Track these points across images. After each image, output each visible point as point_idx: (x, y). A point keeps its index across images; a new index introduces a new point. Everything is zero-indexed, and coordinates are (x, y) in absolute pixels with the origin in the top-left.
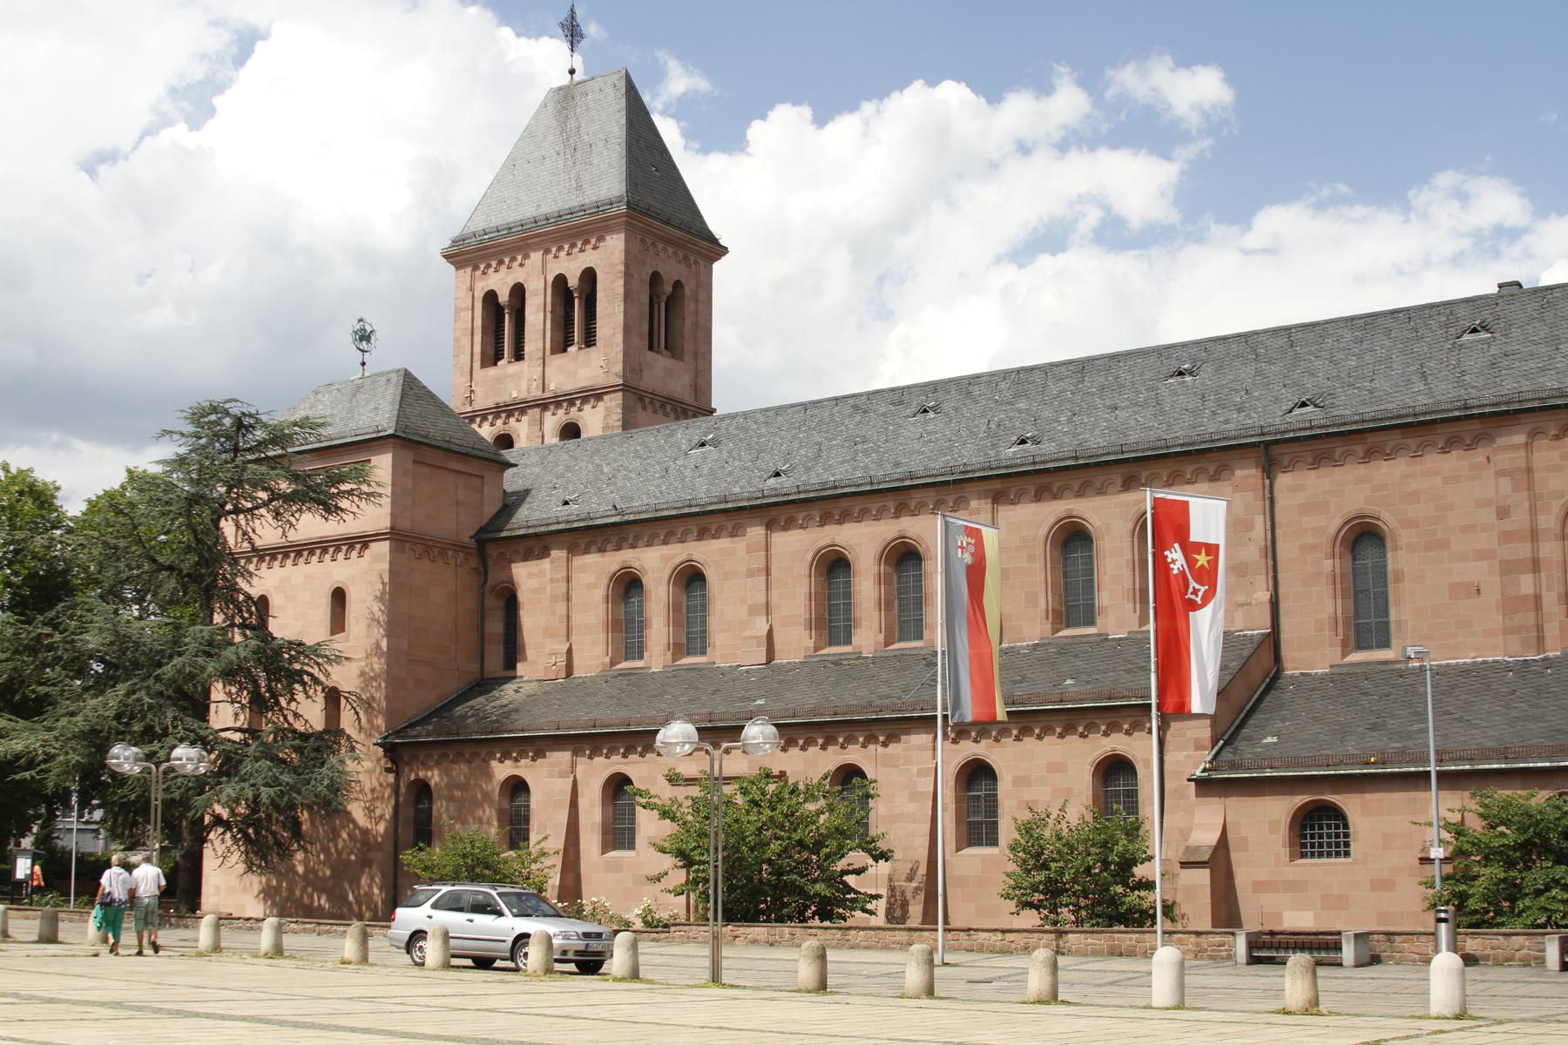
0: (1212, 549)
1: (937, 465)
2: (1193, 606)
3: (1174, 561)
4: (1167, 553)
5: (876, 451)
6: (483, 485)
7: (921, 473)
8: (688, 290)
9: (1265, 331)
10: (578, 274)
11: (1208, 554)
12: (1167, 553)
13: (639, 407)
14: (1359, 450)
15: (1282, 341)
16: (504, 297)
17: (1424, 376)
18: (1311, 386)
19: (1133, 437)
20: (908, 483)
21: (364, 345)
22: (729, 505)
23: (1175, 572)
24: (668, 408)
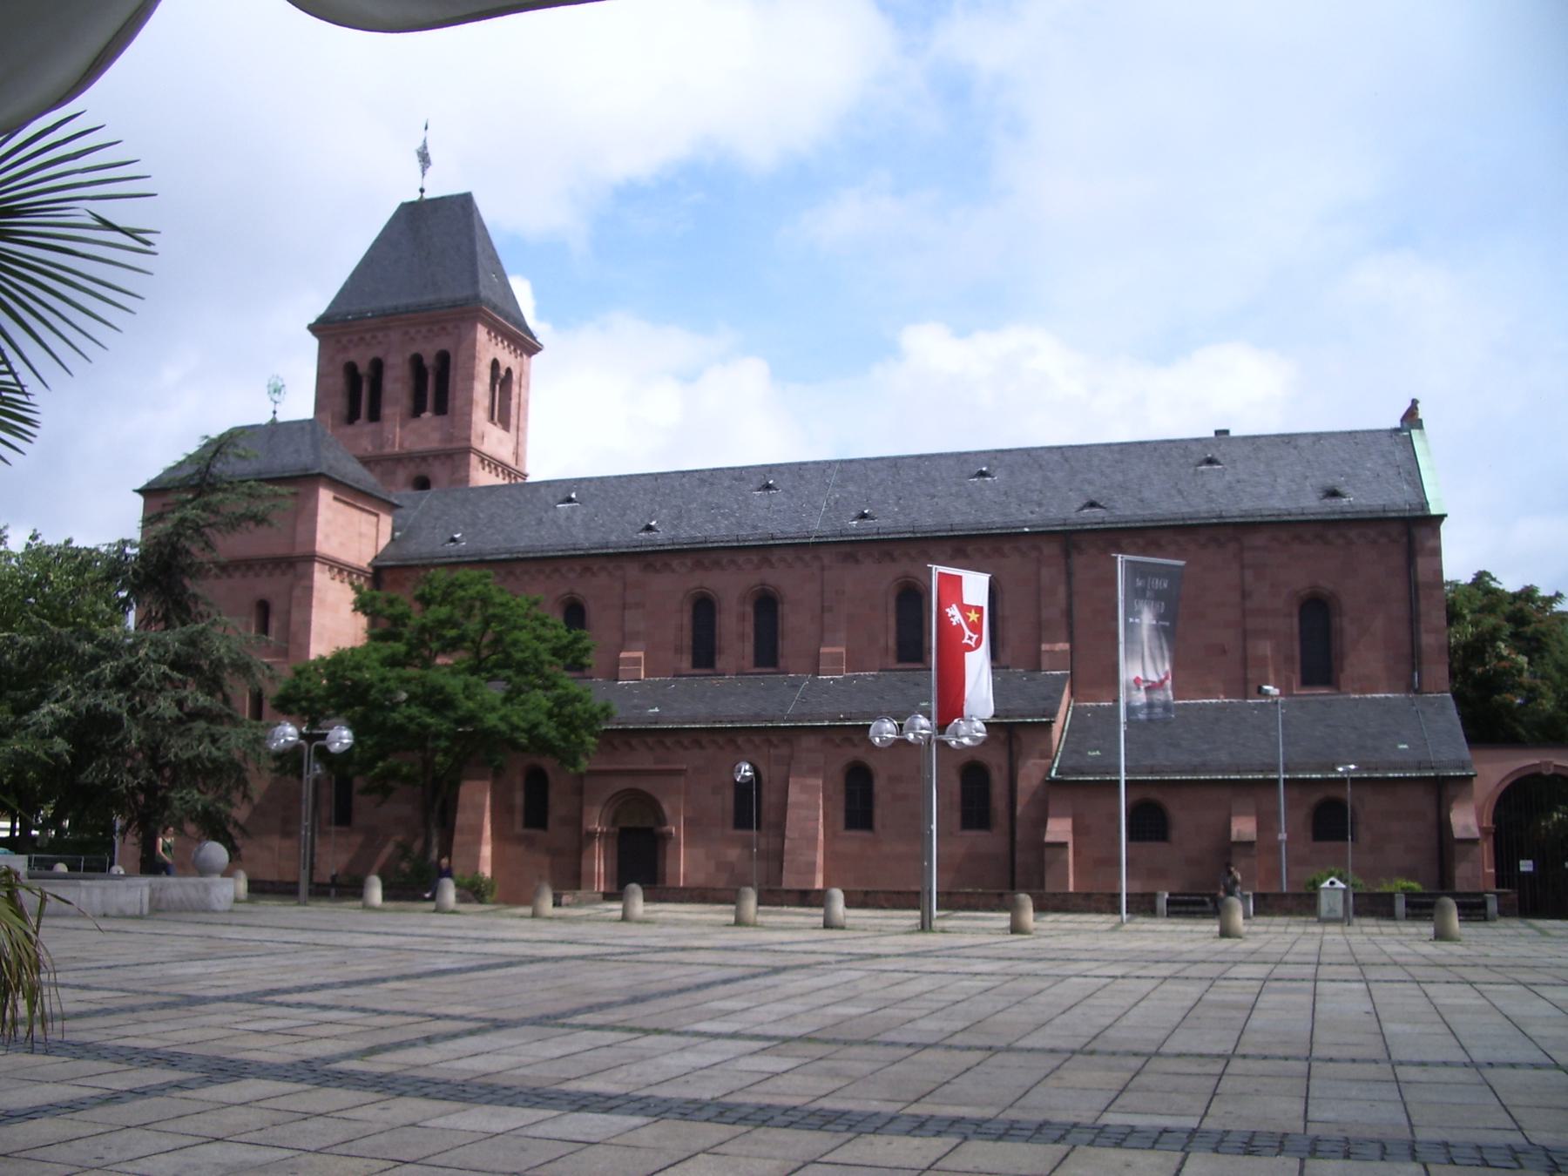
0: (979, 610)
1: (792, 530)
2: (970, 648)
3: (953, 616)
4: (948, 610)
5: (733, 516)
6: (378, 521)
7: (779, 535)
8: (515, 377)
9: (1042, 448)
10: (433, 354)
11: (976, 613)
12: (948, 610)
13: (480, 466)
14: (1141, 542)
15: (1056, 457)
16: (429, 361)
17: (1180, 492)
18: (1091, 492)
19: (957, 519)
20: (771, 542)
21: (276, 397)
22: (611, 551)
23: (954, 624)
24: (500, 469)
